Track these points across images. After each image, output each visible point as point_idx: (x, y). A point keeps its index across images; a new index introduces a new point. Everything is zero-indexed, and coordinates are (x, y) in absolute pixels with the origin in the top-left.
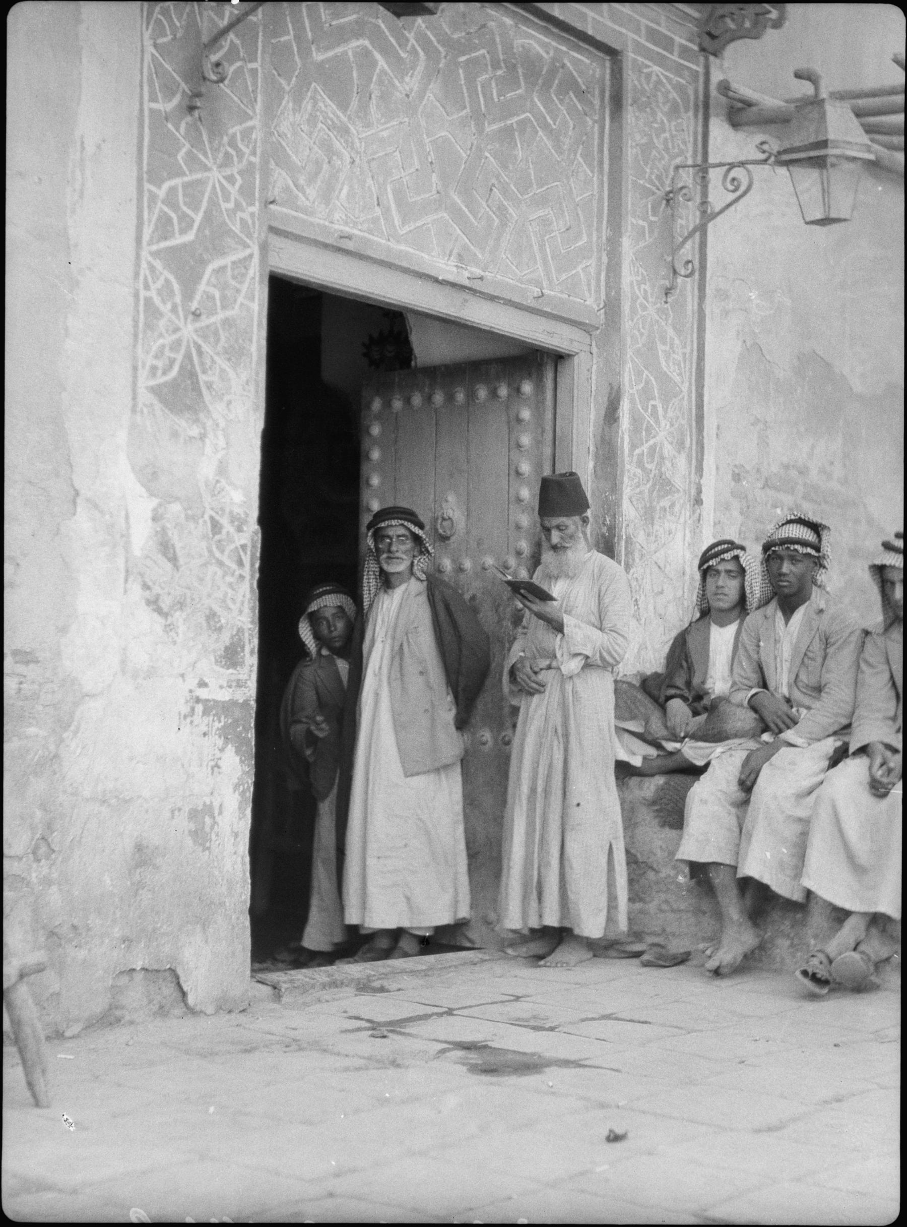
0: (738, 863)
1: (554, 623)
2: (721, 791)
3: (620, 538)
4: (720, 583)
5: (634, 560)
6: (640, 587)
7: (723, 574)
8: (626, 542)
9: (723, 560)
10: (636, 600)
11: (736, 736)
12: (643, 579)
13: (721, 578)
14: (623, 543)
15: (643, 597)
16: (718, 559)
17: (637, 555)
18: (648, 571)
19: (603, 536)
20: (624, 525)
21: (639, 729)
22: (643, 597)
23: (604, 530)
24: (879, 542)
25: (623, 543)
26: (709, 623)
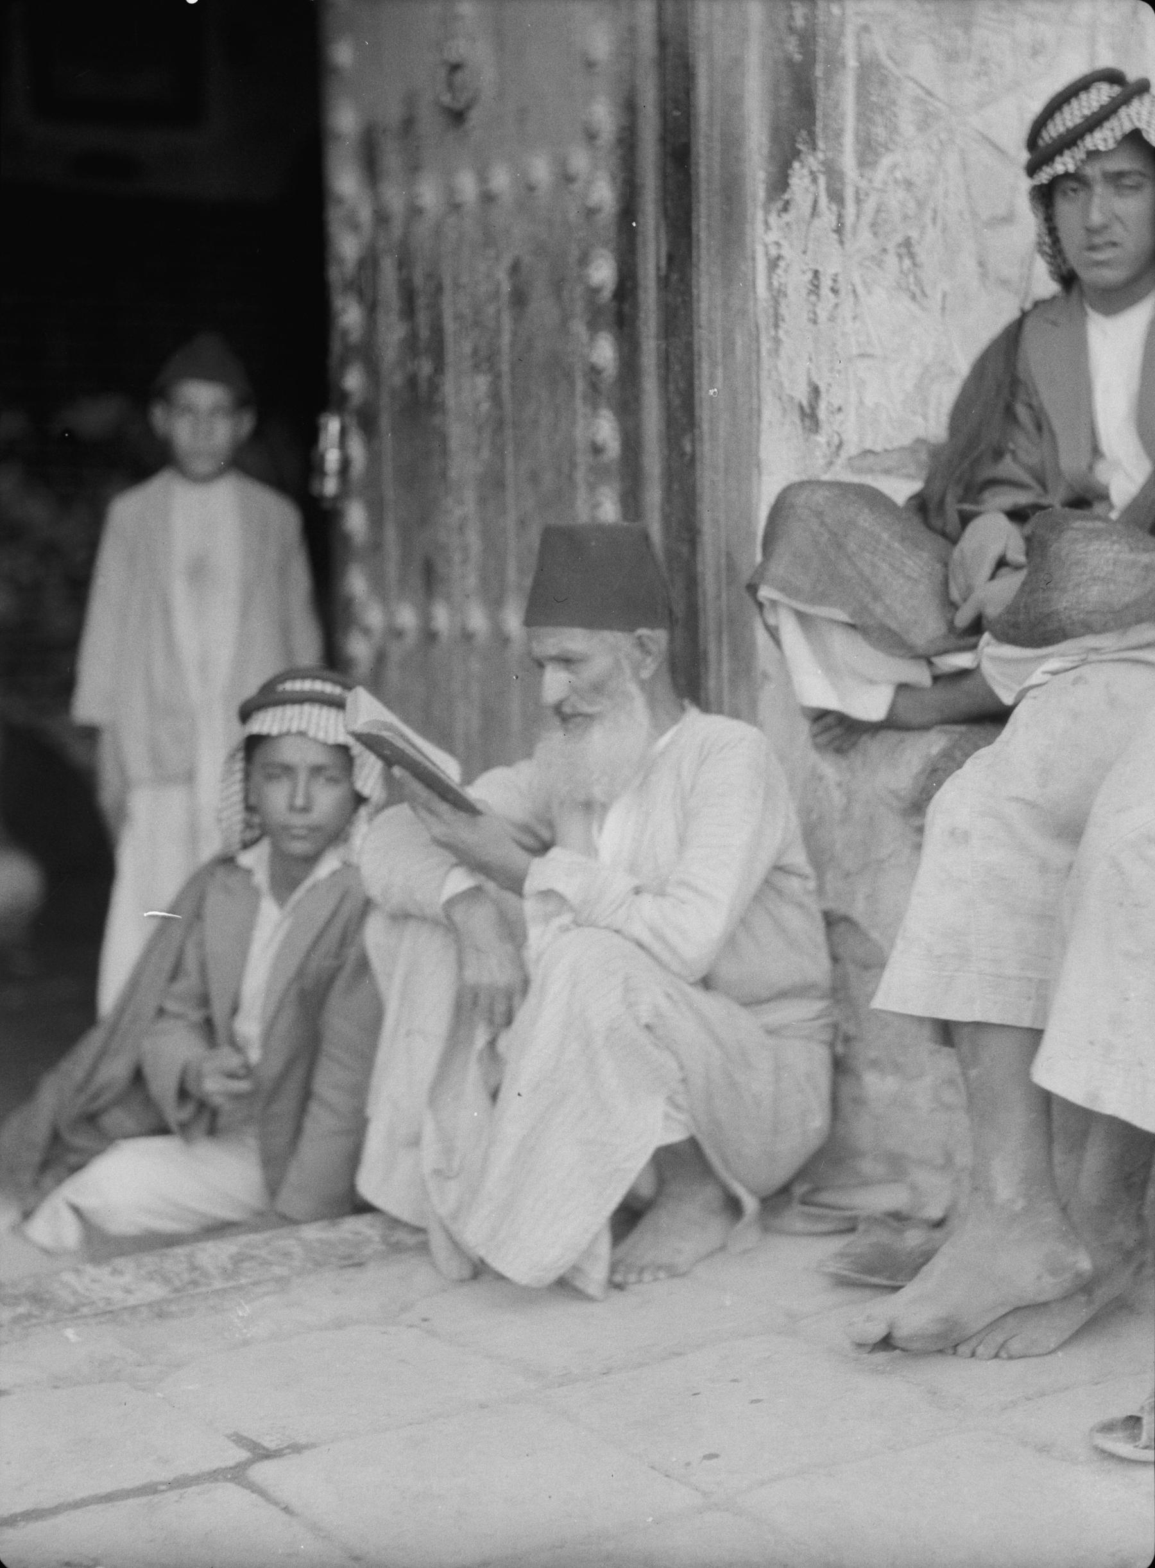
0: (1042, 993)
1: (626, 307)
2: (1017, 799)
3: (836, 63)
4: (1096, 218)
5: (893, 130)
6: (921, 204)
7: (1099, 189)
8: (863, 79)
9: (1093, 155)
10: (907, 243)
11: (1088, 629)
12: (932, 182)
13: (1096, 201)
14: (848, 83)
15: (932, 234)
16: (1079, 153)
17: (907, 120)
18: (952, 160)
19: (789, 63)
20: (850, 29)
21: (843, 616)
22: (932, 234)
23: (792, 45)
24: (697, 725)
25: (848, 83)
26: (1083, 309)
